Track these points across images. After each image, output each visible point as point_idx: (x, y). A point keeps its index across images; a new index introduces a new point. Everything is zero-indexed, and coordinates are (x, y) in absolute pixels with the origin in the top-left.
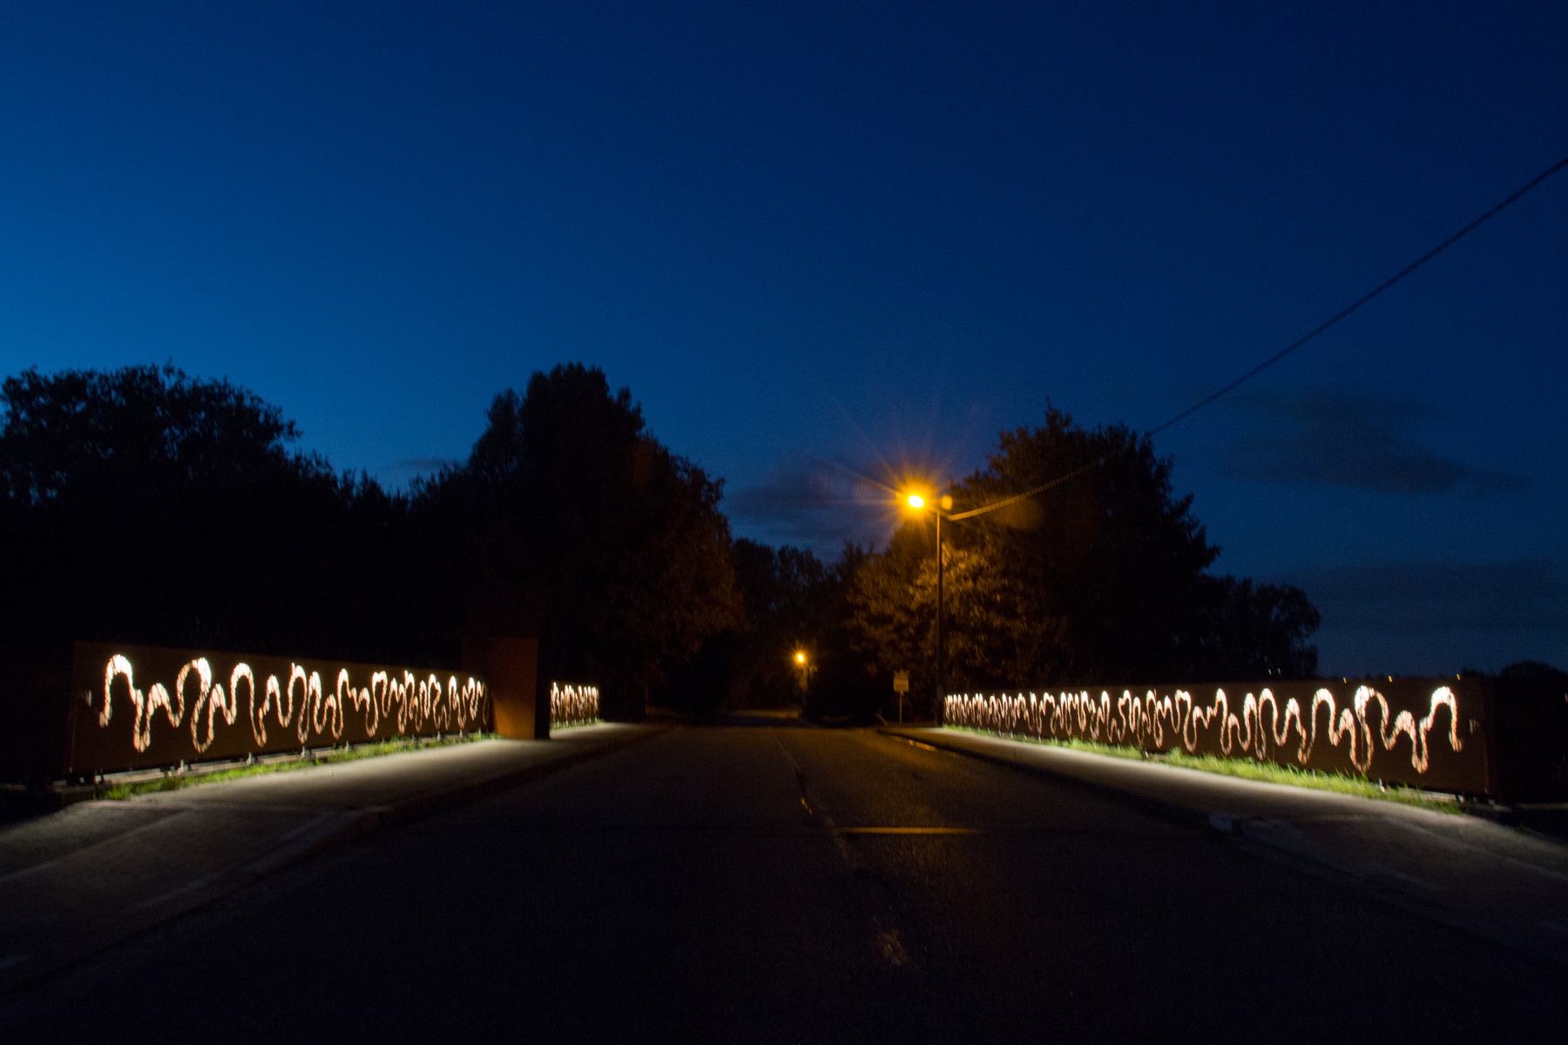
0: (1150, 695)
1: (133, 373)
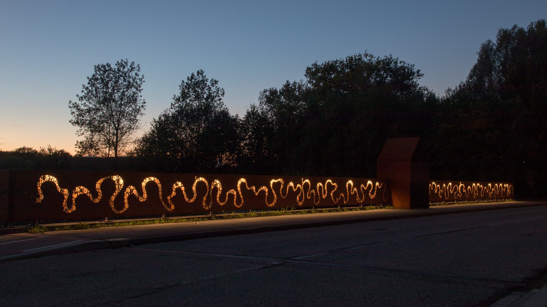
0: (80, 187)
1: (351, 59)
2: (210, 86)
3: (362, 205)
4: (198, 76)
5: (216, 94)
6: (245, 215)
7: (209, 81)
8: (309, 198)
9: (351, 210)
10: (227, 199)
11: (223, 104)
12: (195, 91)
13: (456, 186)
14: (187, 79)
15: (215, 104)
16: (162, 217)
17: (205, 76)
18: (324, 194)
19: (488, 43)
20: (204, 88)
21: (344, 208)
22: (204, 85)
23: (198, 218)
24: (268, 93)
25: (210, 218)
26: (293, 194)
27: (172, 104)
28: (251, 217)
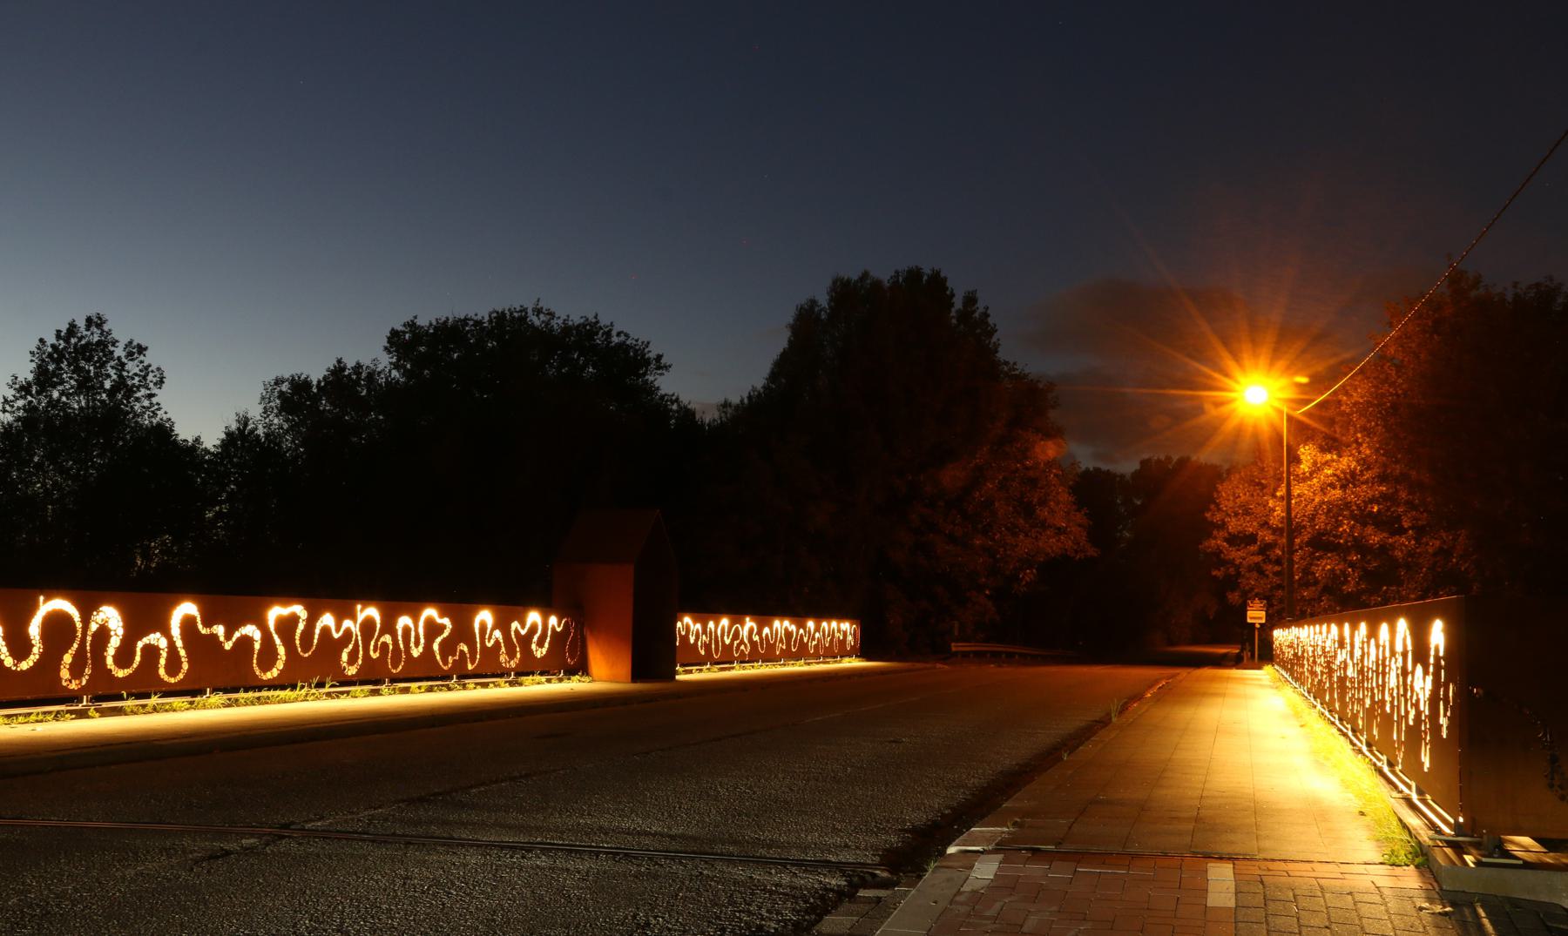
2: (124, 360)
3: (455, 676)
4: (87, 330)
5: (140, 381)
6: (191, 703)
7: (121, 345)
8: (374, 655)
9: (485, 685)
10: (138, 658)
11: (159, 409)
12: (78, 370)
13: (737, 628)
14: (55, 336)
15: (137, 407)
16: (82, 702)
17: (109, 333)
18: (417, 644)
19: (809, 304)
20: (107, 362)
21: (467, 681)
22: (104, 356)
23: (45, 713)
24: (285, 387)
25: (82, 714)
26: (330, 646)
27: (6, 401)
28: (208, 708)
